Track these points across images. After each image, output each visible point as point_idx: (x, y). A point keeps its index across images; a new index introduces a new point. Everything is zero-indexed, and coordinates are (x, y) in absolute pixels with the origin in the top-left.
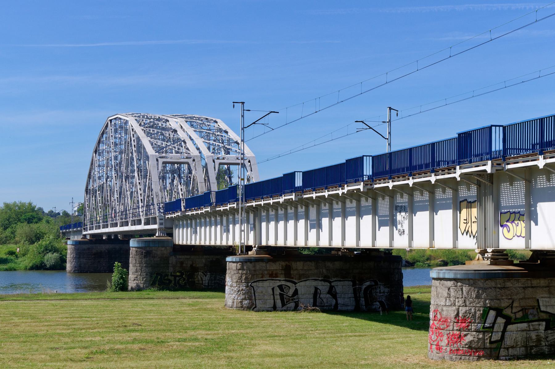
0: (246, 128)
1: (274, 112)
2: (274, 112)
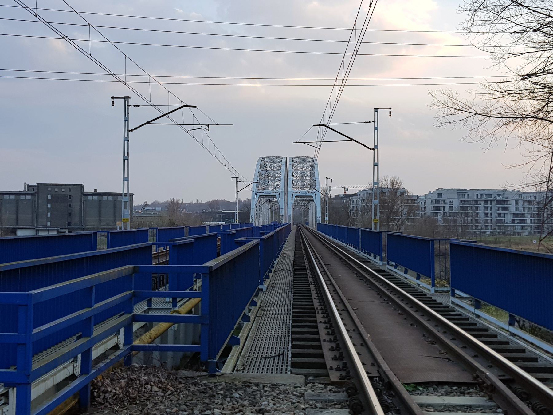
0: (132, 130)
1: (187, 106)
2: (187, 106)
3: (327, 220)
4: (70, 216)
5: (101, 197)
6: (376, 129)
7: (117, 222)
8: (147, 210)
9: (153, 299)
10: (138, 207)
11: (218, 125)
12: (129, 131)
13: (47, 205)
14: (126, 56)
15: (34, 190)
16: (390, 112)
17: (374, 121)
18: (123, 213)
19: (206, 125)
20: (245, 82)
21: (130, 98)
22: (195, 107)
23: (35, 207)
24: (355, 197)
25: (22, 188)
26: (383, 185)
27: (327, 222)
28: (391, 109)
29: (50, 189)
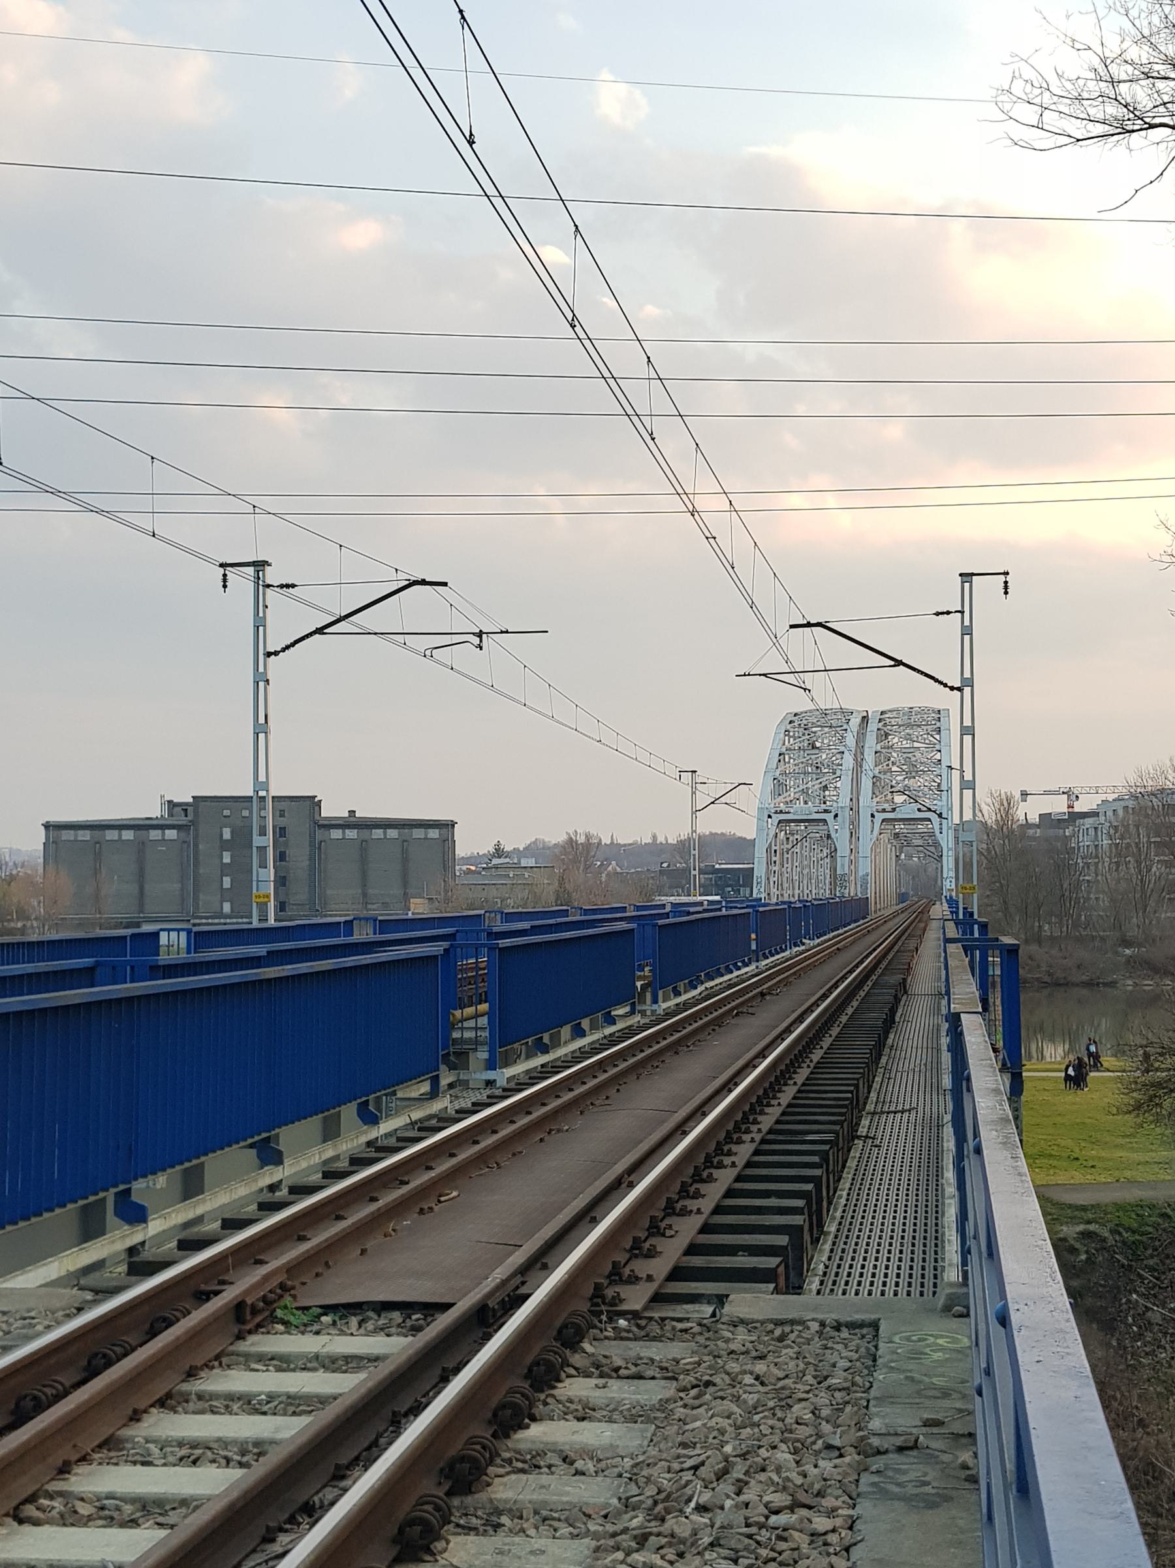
0: (276, 653)
1: (423, 582)
2: (423, 582)
4: (284, 885)
5: (366, 832)
6: (967, 631)
7: (412, 900)
8: (496, 867)
10: (467, 860)
11: (507, 632)
12: (269, 654)
13: (222, 859)
14: (153, 458)
15: (186, 816)
16: (1006, 582)
17: (960, 609)
18: (255, 878)
19: (473, 634)
20: (795, 500)
21: (270, 565)
22: (445, 584)
23: (188, 861)
24: (1089, 821)
25: (154, 810)
26: (1168, 783)
28: (1007, 573)
29: (227, 812)
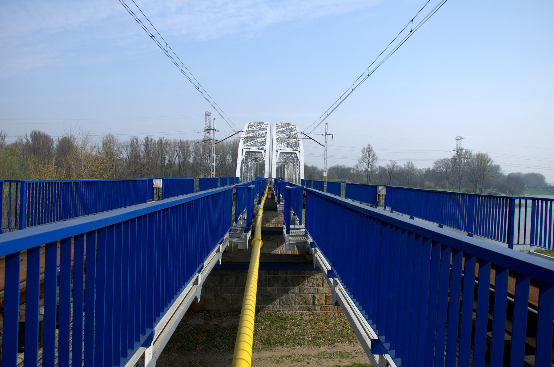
3: (326, 175)
9: (521, 200)
27: (325, 178)
